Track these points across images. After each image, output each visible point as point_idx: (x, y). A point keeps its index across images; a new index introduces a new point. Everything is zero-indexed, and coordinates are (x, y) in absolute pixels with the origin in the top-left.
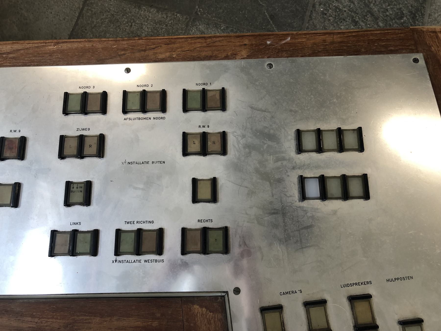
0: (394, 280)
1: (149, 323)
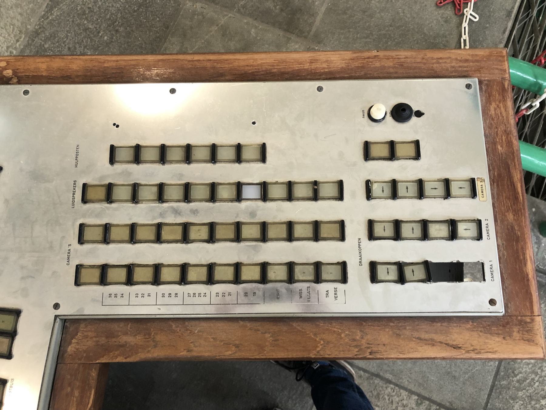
0: (77, 161)
1: (75, 399)
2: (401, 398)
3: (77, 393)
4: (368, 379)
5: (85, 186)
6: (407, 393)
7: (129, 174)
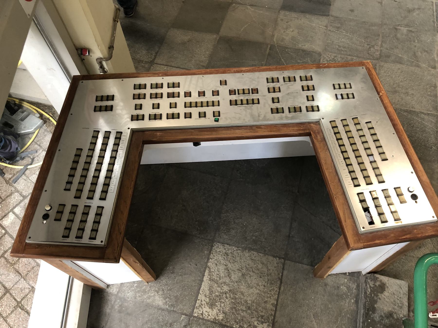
2: (274, 295)
3: (302, 128)
4: (279, 278)
5: (357, 118)
6: (276, 298)
7: (365, 127)
